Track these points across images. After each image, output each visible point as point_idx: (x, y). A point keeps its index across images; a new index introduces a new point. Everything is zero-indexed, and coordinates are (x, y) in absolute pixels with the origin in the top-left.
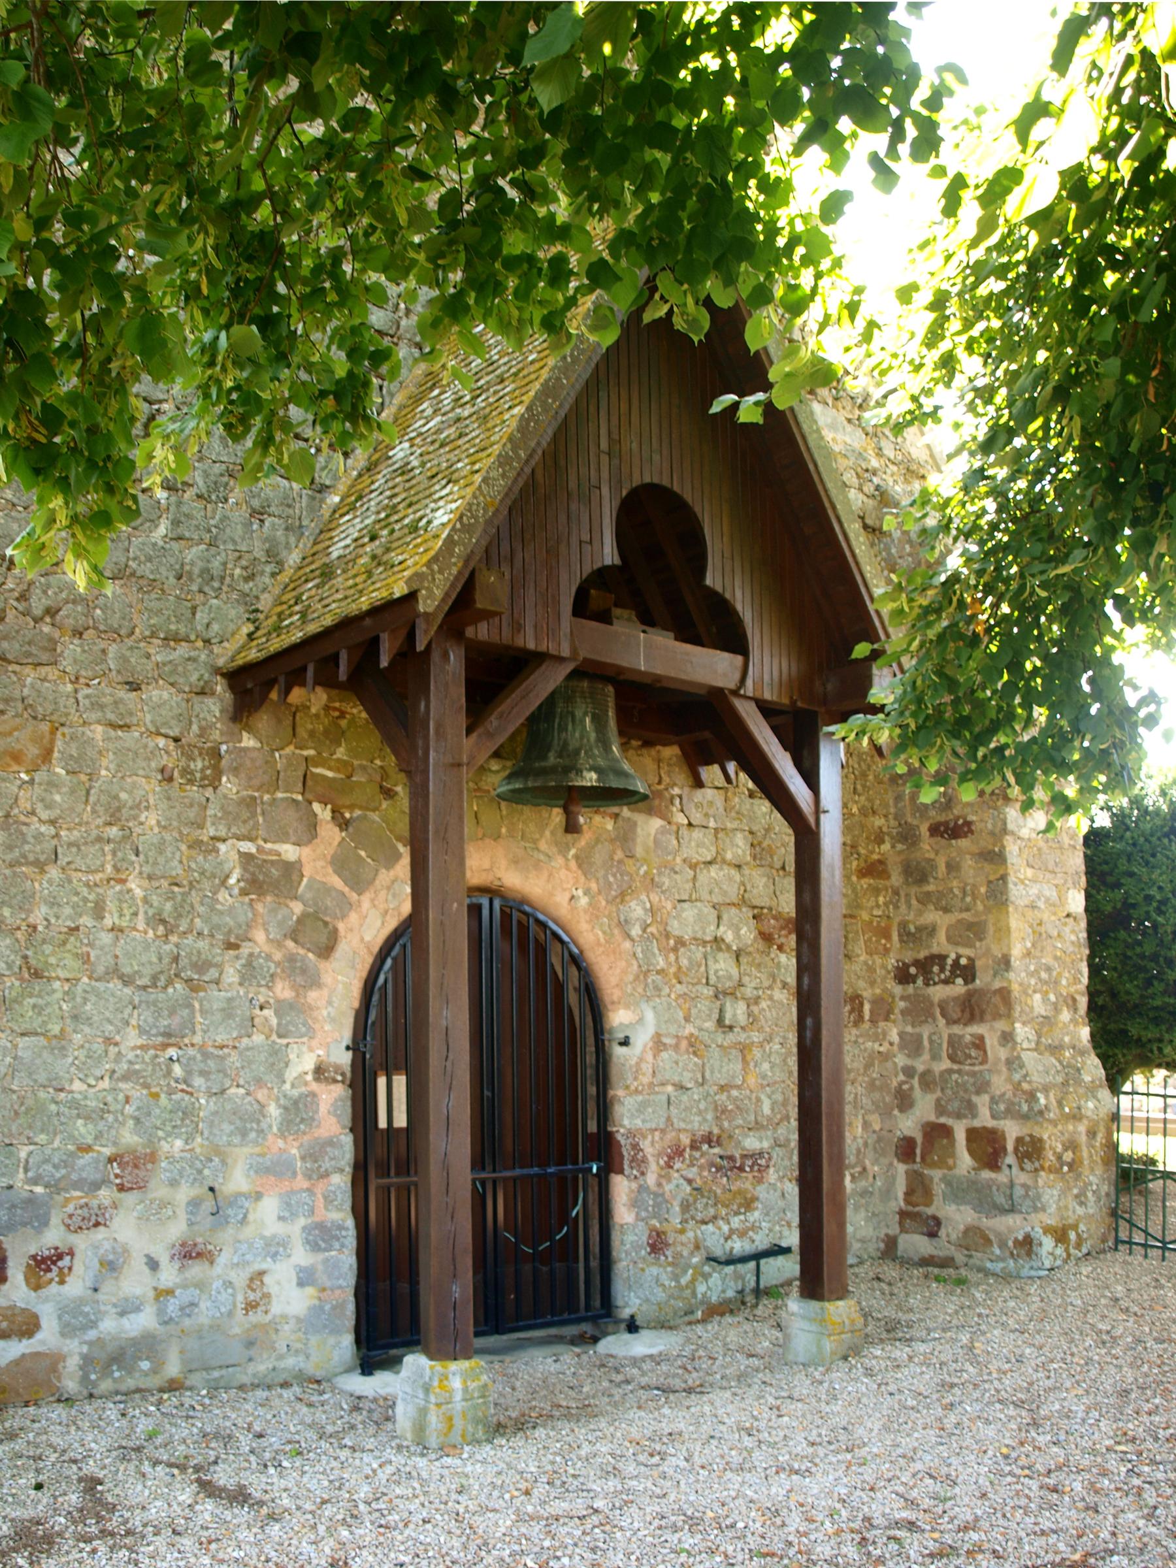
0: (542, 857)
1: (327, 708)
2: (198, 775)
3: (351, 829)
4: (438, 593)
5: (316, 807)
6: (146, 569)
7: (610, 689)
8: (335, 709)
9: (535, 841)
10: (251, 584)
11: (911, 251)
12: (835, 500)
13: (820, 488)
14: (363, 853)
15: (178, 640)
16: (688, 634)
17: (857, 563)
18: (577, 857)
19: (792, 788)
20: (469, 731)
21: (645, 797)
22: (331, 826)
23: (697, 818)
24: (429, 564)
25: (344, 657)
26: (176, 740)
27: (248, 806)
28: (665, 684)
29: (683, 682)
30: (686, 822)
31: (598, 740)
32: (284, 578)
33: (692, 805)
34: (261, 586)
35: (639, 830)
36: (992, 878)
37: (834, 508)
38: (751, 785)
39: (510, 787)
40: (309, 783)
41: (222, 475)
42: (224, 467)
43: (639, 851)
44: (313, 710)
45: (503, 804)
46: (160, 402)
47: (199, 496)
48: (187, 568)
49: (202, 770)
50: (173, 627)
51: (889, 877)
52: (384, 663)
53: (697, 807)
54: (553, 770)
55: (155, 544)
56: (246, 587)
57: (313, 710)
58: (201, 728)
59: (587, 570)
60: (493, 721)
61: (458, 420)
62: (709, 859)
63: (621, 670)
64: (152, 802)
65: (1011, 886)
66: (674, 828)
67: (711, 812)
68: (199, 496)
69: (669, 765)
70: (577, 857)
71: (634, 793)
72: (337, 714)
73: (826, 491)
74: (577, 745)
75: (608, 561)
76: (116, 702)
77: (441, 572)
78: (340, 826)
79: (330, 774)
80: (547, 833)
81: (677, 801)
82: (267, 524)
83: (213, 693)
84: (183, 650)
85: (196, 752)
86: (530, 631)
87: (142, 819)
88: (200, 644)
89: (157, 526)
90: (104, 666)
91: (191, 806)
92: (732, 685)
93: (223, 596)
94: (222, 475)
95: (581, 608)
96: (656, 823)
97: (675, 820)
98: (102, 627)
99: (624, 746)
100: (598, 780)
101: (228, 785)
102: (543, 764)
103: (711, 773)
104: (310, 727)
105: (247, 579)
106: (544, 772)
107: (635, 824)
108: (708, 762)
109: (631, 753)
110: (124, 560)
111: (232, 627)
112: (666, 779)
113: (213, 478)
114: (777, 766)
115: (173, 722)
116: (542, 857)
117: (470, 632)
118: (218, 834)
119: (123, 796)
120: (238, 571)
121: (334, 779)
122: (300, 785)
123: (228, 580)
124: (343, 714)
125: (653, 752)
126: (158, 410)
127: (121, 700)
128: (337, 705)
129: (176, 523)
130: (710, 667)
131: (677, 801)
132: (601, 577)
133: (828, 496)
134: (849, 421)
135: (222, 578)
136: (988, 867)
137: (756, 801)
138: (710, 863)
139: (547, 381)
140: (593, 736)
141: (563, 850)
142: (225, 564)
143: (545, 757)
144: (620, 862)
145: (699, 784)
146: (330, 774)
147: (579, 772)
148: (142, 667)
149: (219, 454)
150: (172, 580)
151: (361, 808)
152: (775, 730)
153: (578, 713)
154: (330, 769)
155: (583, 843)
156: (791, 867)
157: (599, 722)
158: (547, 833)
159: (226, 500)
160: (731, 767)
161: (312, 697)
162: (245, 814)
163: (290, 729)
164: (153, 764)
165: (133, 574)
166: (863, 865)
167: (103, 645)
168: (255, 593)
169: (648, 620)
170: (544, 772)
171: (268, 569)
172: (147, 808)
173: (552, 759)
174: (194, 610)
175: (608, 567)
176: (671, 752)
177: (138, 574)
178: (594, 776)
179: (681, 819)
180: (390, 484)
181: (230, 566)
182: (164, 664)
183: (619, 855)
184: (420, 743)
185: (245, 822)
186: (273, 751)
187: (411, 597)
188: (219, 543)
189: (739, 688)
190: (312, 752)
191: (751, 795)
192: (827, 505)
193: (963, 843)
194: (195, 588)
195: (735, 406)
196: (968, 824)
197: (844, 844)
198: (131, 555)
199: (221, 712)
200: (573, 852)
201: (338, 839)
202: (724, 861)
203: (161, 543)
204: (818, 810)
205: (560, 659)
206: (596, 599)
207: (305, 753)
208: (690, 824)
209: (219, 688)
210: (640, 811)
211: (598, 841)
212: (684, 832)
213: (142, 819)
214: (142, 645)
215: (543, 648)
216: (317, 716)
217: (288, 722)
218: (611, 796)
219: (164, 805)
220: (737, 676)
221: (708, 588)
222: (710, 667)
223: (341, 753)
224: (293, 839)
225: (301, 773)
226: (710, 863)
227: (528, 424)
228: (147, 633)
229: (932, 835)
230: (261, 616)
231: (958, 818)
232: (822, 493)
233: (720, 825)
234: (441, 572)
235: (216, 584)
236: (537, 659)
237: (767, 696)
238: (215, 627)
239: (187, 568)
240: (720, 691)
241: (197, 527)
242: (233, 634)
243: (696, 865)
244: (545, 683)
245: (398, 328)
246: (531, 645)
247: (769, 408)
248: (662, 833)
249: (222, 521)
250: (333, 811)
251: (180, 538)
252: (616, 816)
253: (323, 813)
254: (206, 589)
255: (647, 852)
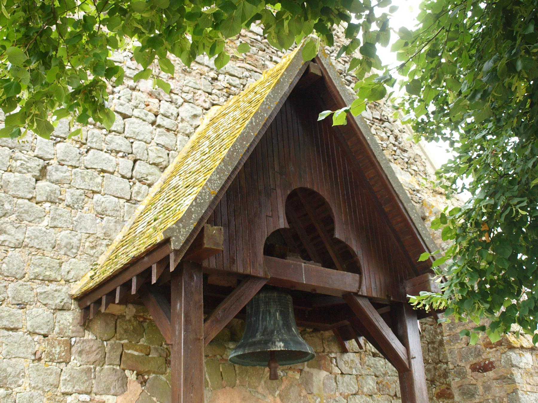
0: (260, 396)
1: (135, 317)
2: (57, 356)
3: (147, 385)
4: (183, 239)
5: (127, 372)
6: (35, 243)
7: (289, 297)
8: (141, 317)
9: (256, 387)
10: (94, 251)
11: (414, 19)
12: (397, 192)
13: (390, 186)
14: (155, 399)
15: (51, 281)
16: (328, 264)
17: (414, 223)
18: (280, 395)
19: (394, 346)
20: (205, 320)
21: (313, 356)
22: (136, 383)
23: (346, 369)
24: (177, 223)
25: (134, 281)
26: (45, 336)
27: (86, 373)
28: (318, 291)
29: (328, 289)
30: (340, 372)
31: (284, 325)
32: (112, 247)
33: (342, 363)
34: (100, 252)
35: (314, 378)
36: (509, 392)
37: (398, 196)
38: (374, 350)
39: (236, 354)
40: (124, 358)
41: (81, 195)
42: (82, 191)
43: (315, 390)
44: (127, 318)
45: (237, 366)
46: (50, 159)
47: (68, 206)
48: (58, 242)
49: (59, 353)
50: (48, 273)
51: (453, 398)
52: (154, 281)
53: (345, 364)
54: (259, 342)
55: (40, 230)
56: (92, 252)
57: (127, 318)
58: (60, 329)
59: (272, 230)
60: (219, 312)
61: (202, 161)
62: (354, 392)
63: (293, 284)
64: (27, 372)
65: (520, 396)
66: (333, 376)
67: (353, 366)
68: (68, 206)
69: (328, 341)
70: (280, 395)
71: (307, 354)
72: (141, 319)
73: (393, 188)
74: (273, 328)
75: (282, 226)
76: (10, 315)
77: (184, 227)
78: (141, 383)
79: (136, 353)
80: (263, 382)
81: (334, 361)
82: (105, 219)
83: (69, 310)
84: (53, 286)
85: (56, 343)
86: (239, 263)
87: (20, 383)
88: (63, 282)
89: (42, 221)
90: (4, 295)
91: (51, 374)
92: (355, 290)
93: (78, 256)
94: (81, 195)
95: (269, 250)
96: (324, 374)
97: (334, 371)
98: (6, 274)
99: (303, 333)
100: (284, 347)
101: (75, 361)
102: (254, 340)
103: (351, 344)
104: (125, 327)
105: (92, 248)
106: (254, 344)
107: (312, 374)
108: (349, 339)
109: (306, 336)
110: (23, 238)
111: (82, 273)
112: (327, 350)
113: (76, 197)
114: (384, 333)
115: (44, 326)
116: (260, 396)
117: (205, 264)
118: (67, 391)
119: (9, 370)
120: (87, 244)
121: (138, 356)
122: (118, 360)
123: (81, 248)
124: (145, 319)
125: (319, 335)
126: (48, 164)
127: (13, 314)
128: (142, 314)
129: (54, 219)
130: (341, 281)
131: (334, 361)
132: (278, 233)
133: (395, 191)
134: (402, 169)
135: (78, 247)
136: (506, 387)
137: (377, 359)
138: (355, 394)
139: (242, 134)
140: (281, 322)
141: (272, 392)
142: (80, 240)
143: (254, 336)
144: (305, 397)
145: (344, 351)
146: (136, 353)
147: (274, 343)
148: (26, 295)
149: (80, 185)
150: (49, 249)
151: (154, 373)
152: (382, 315)
153: (272, 311)
154: (136, 350)
155: (283, 387)
156: (399, 394)
157: (285, 315)
158: (263, 382)
159: (83, 208)
160: (362, 340)
161: (127, 310)
162: (84, 378)
163: (113, 328)
164: (30, 350)
165: (26, 246)
166: (439, 391)
167: (5, 283)
168: (96, 255)
169: (307, 258)
170: (254, 344)
171: (105, 242)
172: (23, 376)
173: (259, 337)
174: (61, 264)
175: (282, 229)
176: (328, 334)
177: (30, 245)
178: (282, 344)
179: (337, 370)
180: (168, 195)
181: (83, 241)
182: (41, 294)
183: (304, 393)
184: (177, 328)
185: (84, 383)
186: (103, 341)
187: (166, 241)
188: (77, 229)
189: (358, 291)
190: (126, 341)
191: (374, 355)
192: (395, 195)
193: (491, 374)
194: (62, 252)
195: (331, 115)
196: (491, 363)
197: (427, 380)
198: (27, 235)
199: (73, 319)
200: (278, 392)
201: (140, 391)
202: (363, 393)
203: (44, 229)
204: (409, 358)
205: (257, 278)
206: (277, 246)
207: (122, 342)
208: (342, 373)
209: (73, 307)
210: (314, 367)
211: (291, 386)
212: (339, 377)
213: (20, 383)
214: (29, 283)
215: (248, 272)
216: (130, 321)
217: (112, 324)
218: (292, 357)
219: (34, 375)
220: (357, 285)
221: (337, 239)
222: (341, 281)
223: (142, 341)
224: (113, 392)
225: (119, 353)
226: (355, 394)
227: (233, 154)
228: (32, 277)
229: (473, 371)
230: (98, 267)
231: (486, 360)
232: (391, 189)
233: (358, 373)
234: (184, 227)
235: (74, 251)
236: (244, 279)
237: (374, 295)
238: (72, 273)
239: (58, 242)
240: (349, 293)
241: (66, 221)
242: (82, 277)
243: (348, 395)
244: (251, 291)
245: (177, 127)
246: (241, 270)
247: (349, 116)
248: (327, 379)
249: (80, 218)
250: (138, 374)
251: (55, 227)
252: (301, 371)
253: (131, 376)
254: (69, 253)
255: (320, 390)
